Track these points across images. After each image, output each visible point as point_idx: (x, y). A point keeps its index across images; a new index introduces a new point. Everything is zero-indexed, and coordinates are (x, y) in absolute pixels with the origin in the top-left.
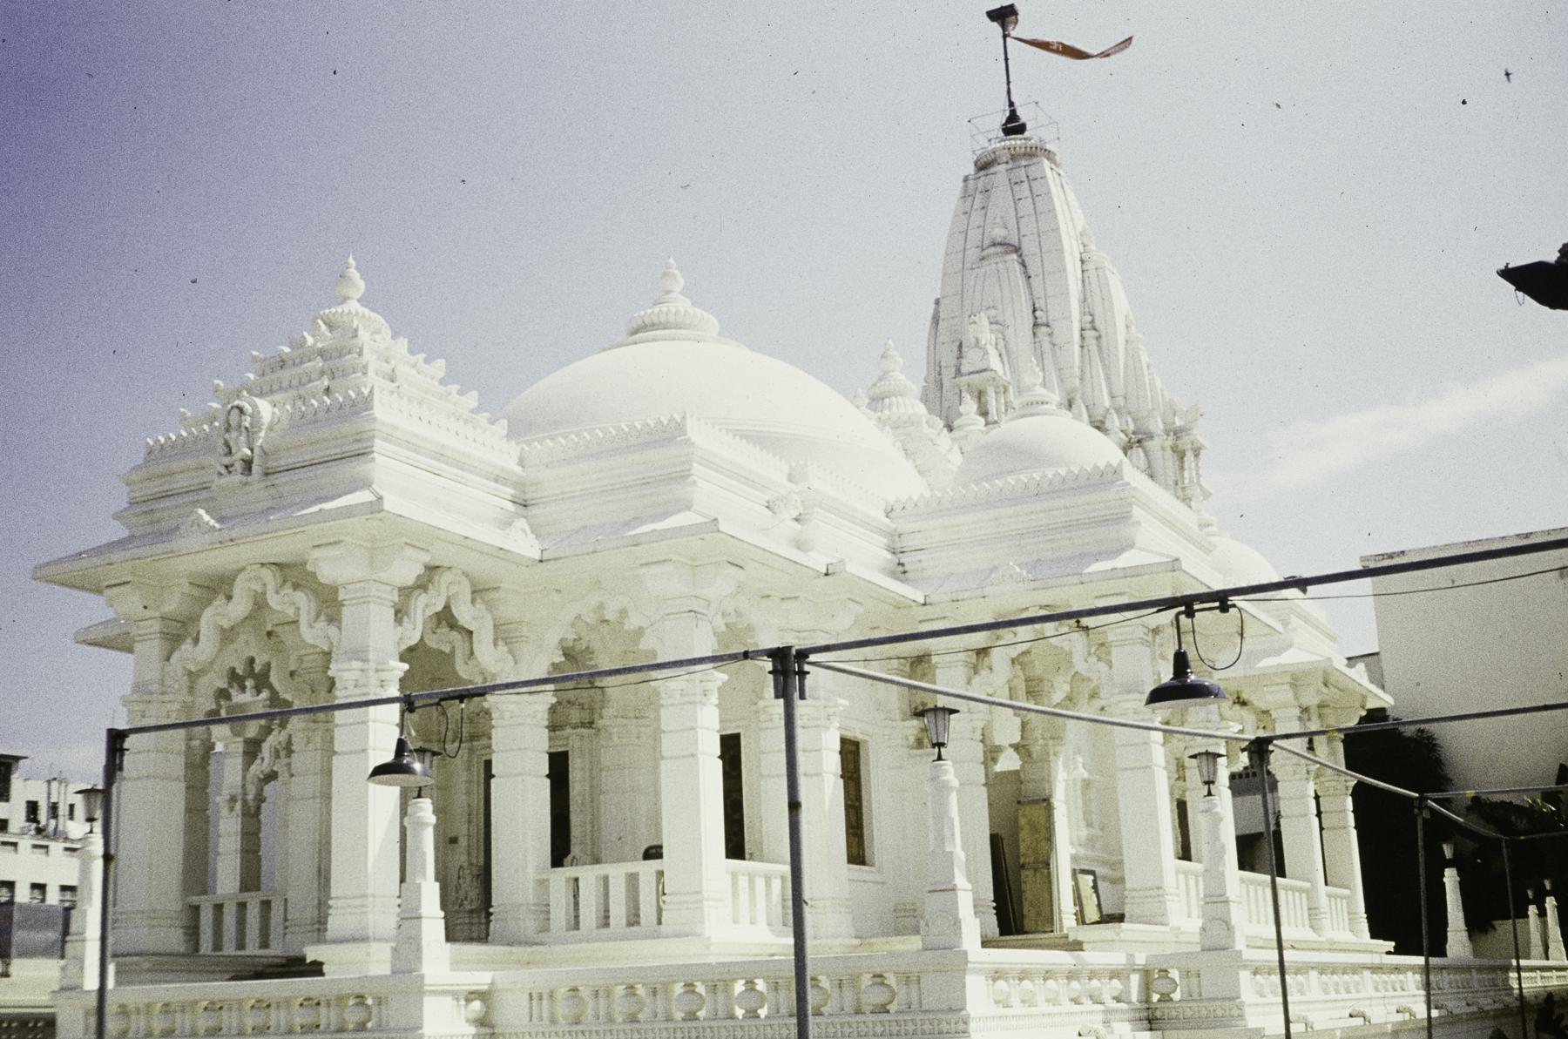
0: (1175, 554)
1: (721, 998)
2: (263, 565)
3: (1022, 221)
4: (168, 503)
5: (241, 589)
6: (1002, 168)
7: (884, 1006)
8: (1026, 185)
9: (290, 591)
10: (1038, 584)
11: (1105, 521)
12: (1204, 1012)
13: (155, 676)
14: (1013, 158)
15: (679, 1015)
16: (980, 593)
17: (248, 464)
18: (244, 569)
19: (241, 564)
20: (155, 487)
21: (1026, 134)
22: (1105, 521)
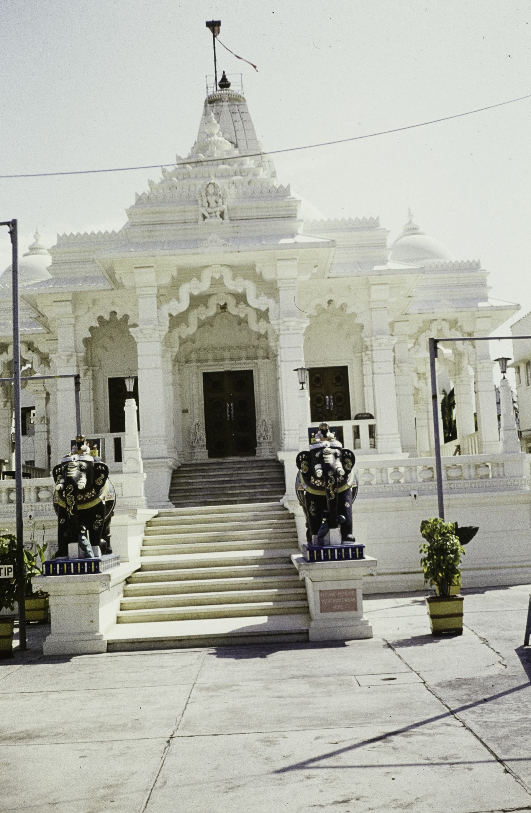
0: (518, 303)
1: (384, 474)
2: (222, 265)
3: (237, 132)
4: (162, 227)
5: (206, 276)
6: (225, 104)
7: (369, 482)
8: (238, 115)
9: (242, 280)
10: (459, 310)
11: (475, 285)
12: (41, 508)
13: (155, 316)
14: (230, 99)
15: (391, 481)
16: (431, 311)
17: (222, 216)
18: (211, 266)
19: (210, 264)
20: (154, 219)
21: (230, 88)
22: (475, 285)
